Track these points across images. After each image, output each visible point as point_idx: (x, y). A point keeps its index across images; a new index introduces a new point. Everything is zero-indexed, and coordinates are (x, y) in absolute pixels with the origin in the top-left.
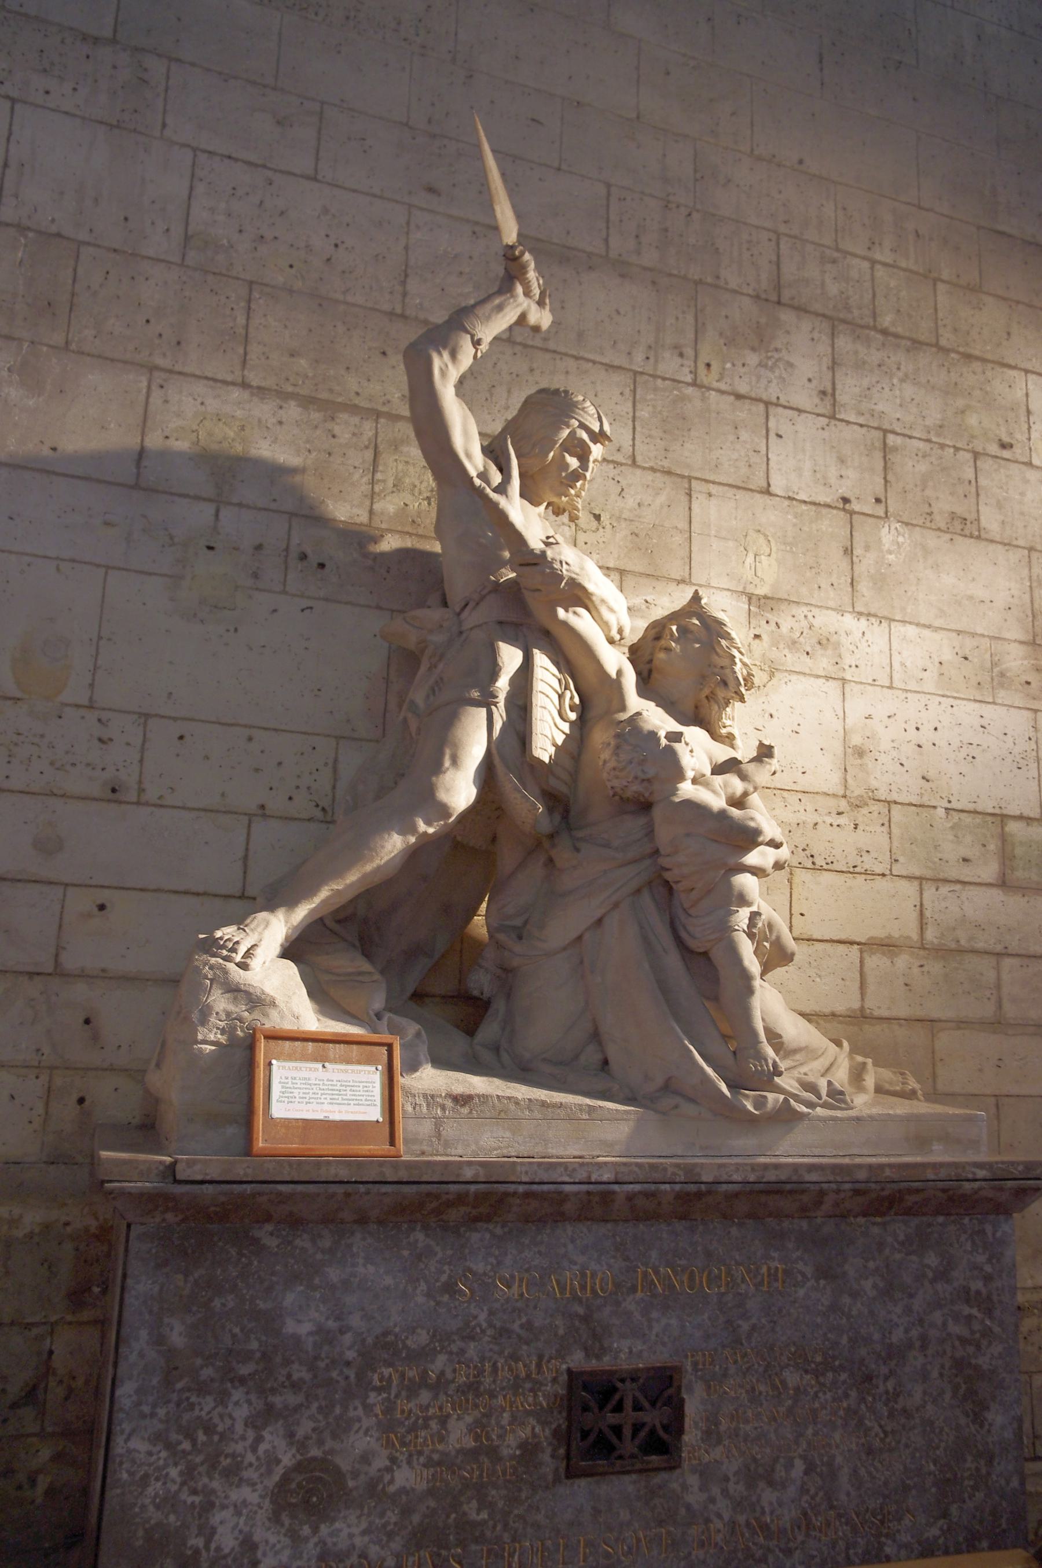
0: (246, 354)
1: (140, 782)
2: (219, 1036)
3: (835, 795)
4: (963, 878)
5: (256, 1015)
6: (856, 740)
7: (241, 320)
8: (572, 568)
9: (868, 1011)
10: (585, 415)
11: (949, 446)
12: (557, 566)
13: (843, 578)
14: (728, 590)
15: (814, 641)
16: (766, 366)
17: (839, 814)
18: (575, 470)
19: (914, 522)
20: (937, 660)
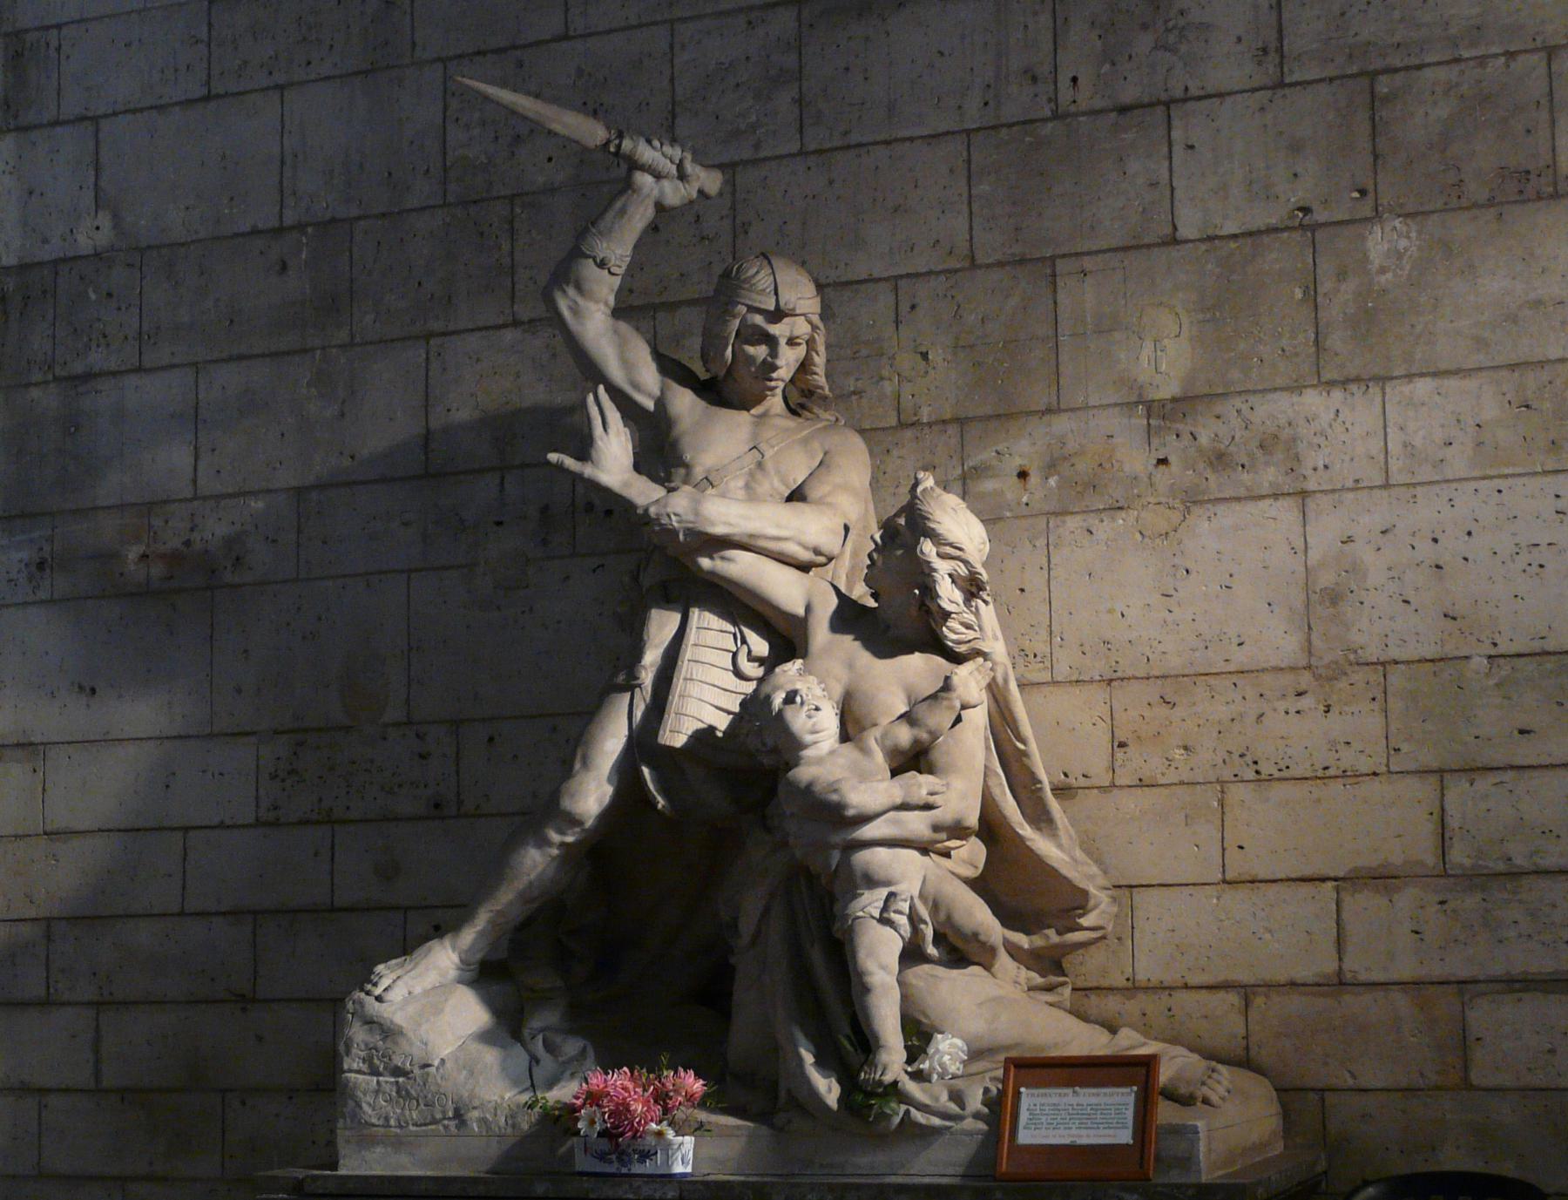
0: (513, 284)
1: (458, 794)
2: (361, 1065)
3: (1293, 669)
4: (1518, 761)
5: (389, 1044)
6: (1326, 579)
7: (506, 247)
8: (684, 518)
9: (1349, 976)
10: (754, 296)
11: (1496, 56)
12: (664, 521)
13: (1301, 337)
14: (1116, 405)
15: (1254, 444)
16: (1166, 48)
17: (1299, 694)
18: (764, 360)
19: (1427, 208)
20: (1471, 422)
